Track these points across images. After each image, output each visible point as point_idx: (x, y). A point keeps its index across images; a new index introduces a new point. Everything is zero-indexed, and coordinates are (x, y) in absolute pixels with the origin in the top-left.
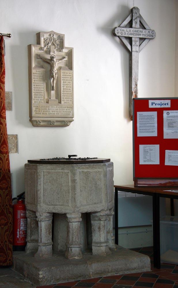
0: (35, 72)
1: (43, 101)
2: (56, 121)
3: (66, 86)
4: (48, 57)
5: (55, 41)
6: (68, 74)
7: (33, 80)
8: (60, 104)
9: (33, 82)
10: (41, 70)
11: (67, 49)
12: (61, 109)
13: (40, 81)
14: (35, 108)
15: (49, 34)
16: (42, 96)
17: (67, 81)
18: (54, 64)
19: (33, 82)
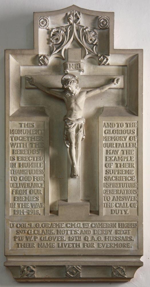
0: (15, 128)
1: (40, 211)
2: (83, 267)
3: (117, 164)
4: (56, 81)
5: (85, 35)
6: (124, 128)
7: (11, 149)
8: (94, 217)
9: (11, 155)
10: (37, 121)
11: (124, 54)
12: (98, 231)
13: (33, 152)
14: (15, 229)
15: (64, 15)
16: (39, 196)
17: (120, 149)
18: (73, 101)
19: (11, 155)
